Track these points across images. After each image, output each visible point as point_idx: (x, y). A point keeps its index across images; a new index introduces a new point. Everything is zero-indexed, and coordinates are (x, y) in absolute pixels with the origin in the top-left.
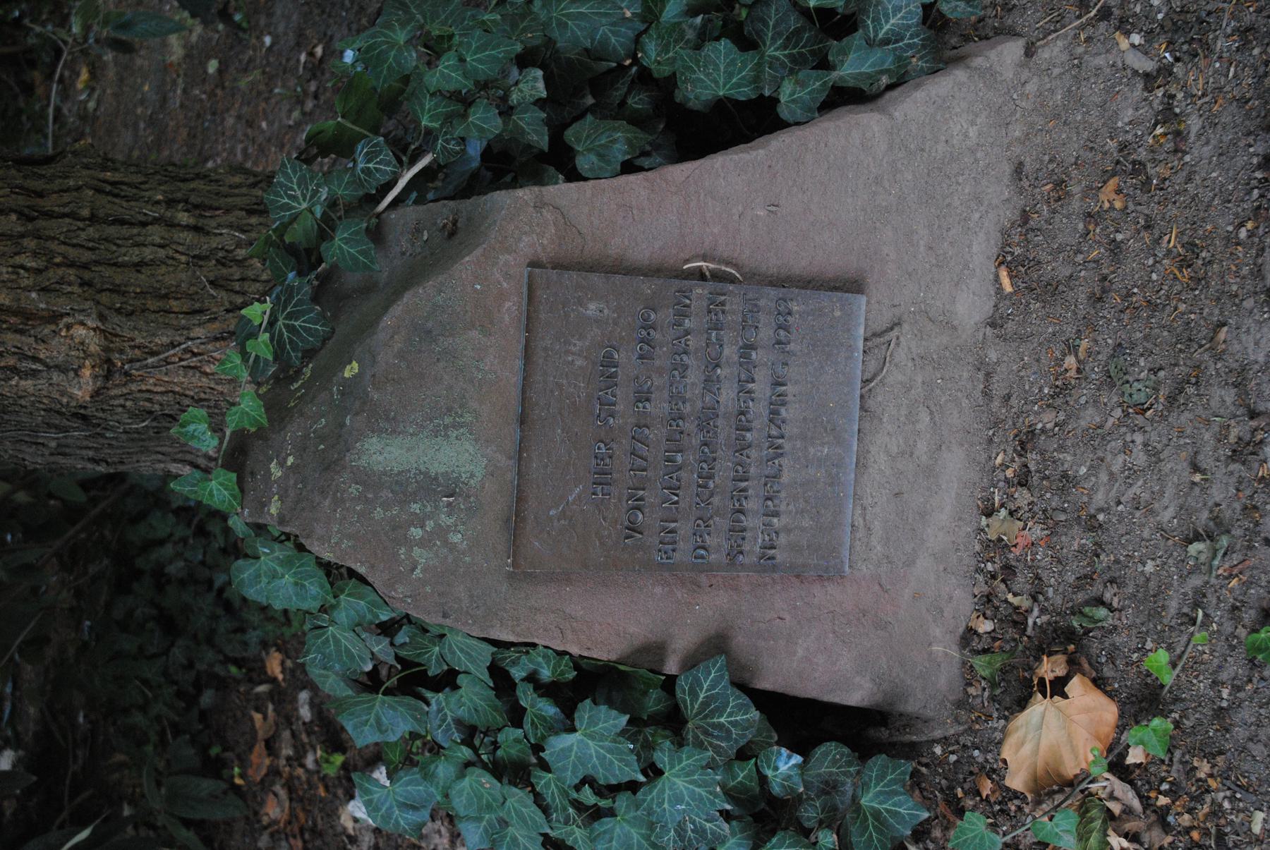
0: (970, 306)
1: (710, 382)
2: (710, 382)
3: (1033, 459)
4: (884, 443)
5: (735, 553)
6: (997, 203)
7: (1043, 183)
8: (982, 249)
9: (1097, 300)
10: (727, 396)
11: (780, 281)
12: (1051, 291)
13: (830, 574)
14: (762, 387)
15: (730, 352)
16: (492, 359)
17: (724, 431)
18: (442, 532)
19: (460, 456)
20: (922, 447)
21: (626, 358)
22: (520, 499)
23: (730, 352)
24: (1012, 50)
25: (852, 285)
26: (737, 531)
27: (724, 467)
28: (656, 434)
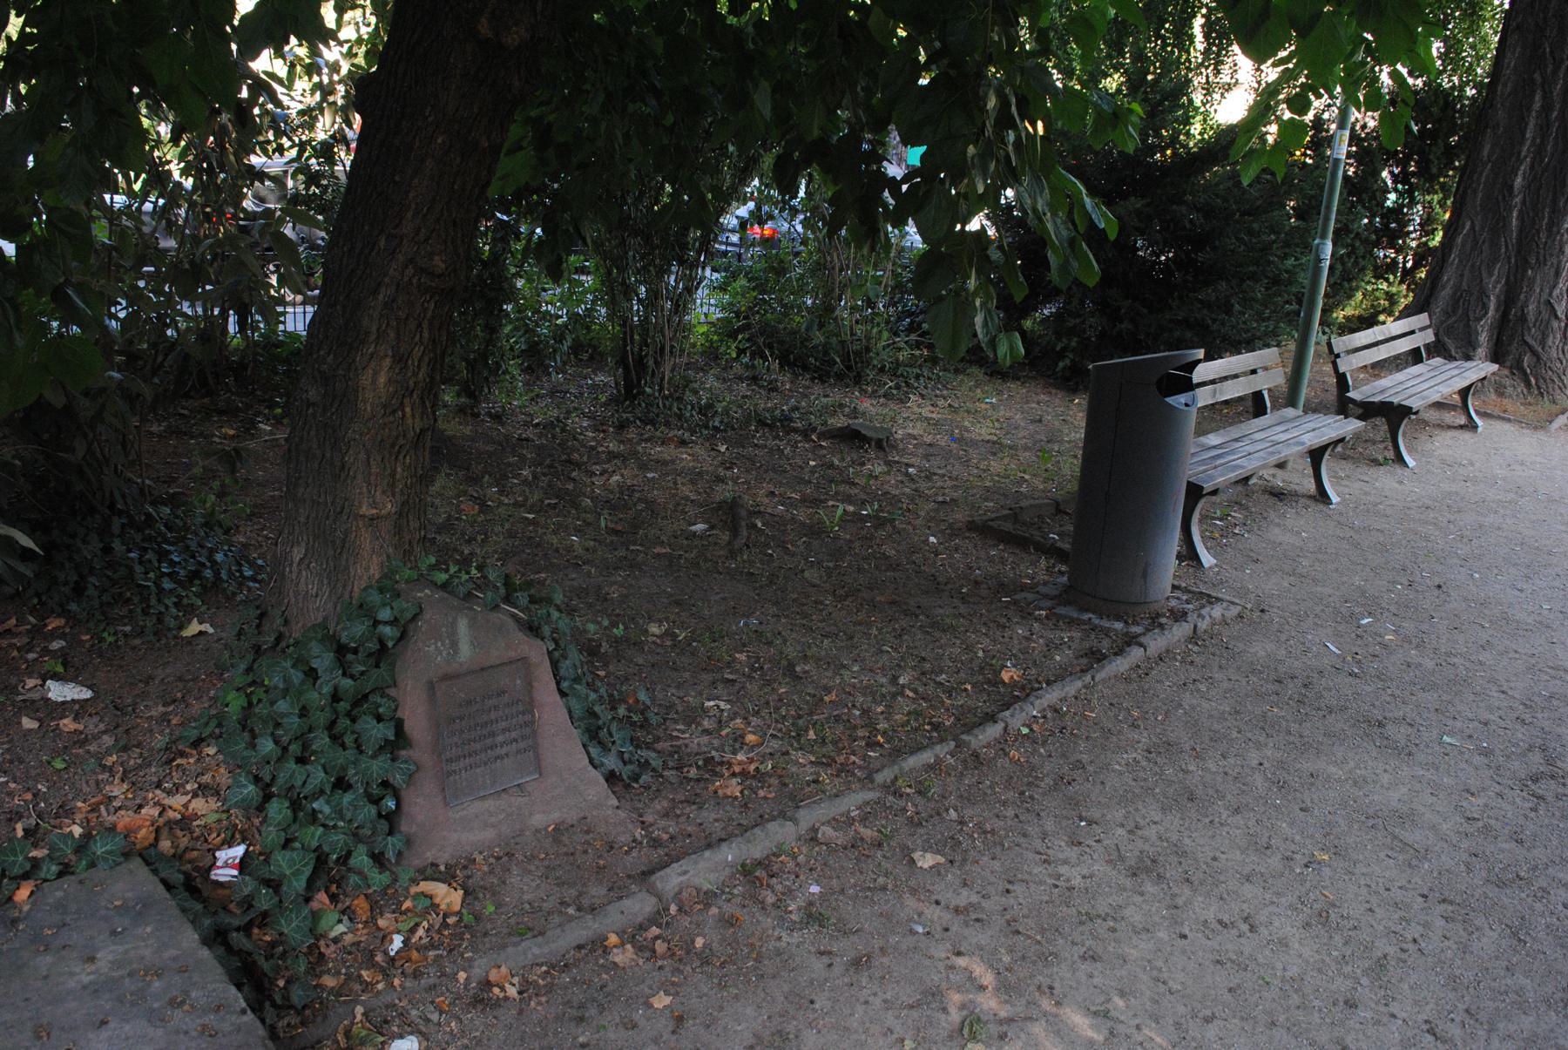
0: (538, 820)
1: (504, 730)
2: (504, 730)
3: (505, 859)
4: (490, 804)
5: (450, 761)
6: (572, 816)
7: (585, 826)
8: (556, 816)
9: (566, 854)
10: (500, 739)
11: (1213, 382)
12: (557, 841)
13: (446, 804)
14: (504, 750)
15: (514, 735)
16: (496, 654)
17: (489, 741)
18: (440, 653)
19: (465, 650)
20: (493, 819)
21: (505, 699)
22: (458, 676)
23: (514, 735)
24: (615, 802)
25: (539, 769)
26: (458, 758)
27: (478, 746)
28: (485, 718)
